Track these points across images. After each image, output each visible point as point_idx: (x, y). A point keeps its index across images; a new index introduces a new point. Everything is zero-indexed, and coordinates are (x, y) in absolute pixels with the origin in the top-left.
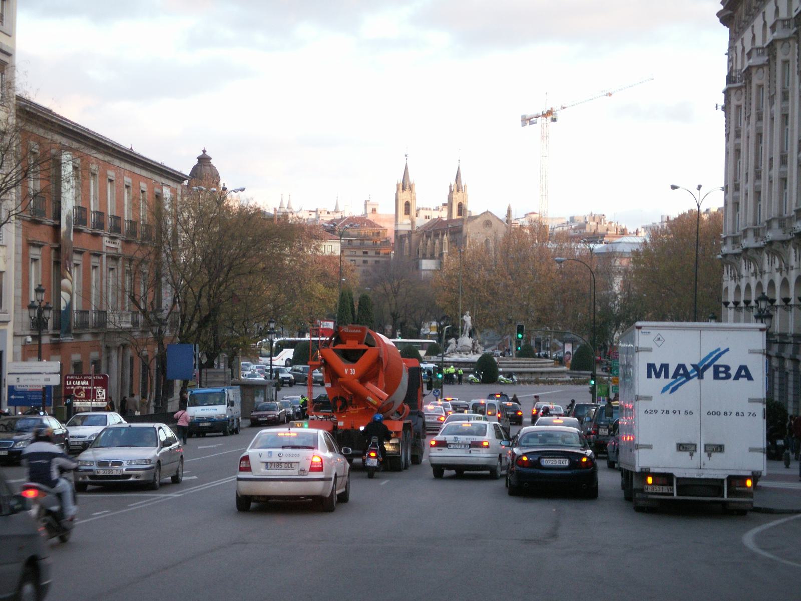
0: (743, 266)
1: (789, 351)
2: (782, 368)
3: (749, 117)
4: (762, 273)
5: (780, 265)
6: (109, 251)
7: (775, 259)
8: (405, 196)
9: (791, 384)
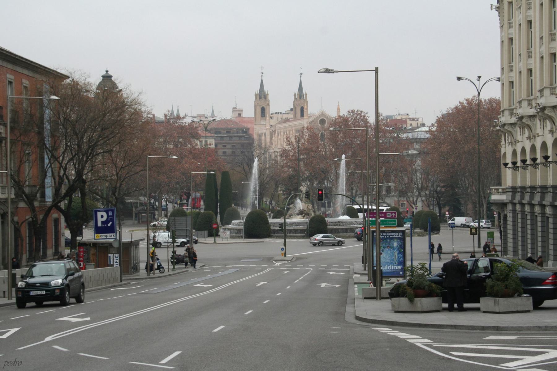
0: (519, 133)
1: (548, 199)
2: (523, 212)
3: (520, 8)
4: (516, 142)
5: (529, 135)
6: (446, 226)
7: (525, 130)
8: (262, 103)
9: (539, 224)
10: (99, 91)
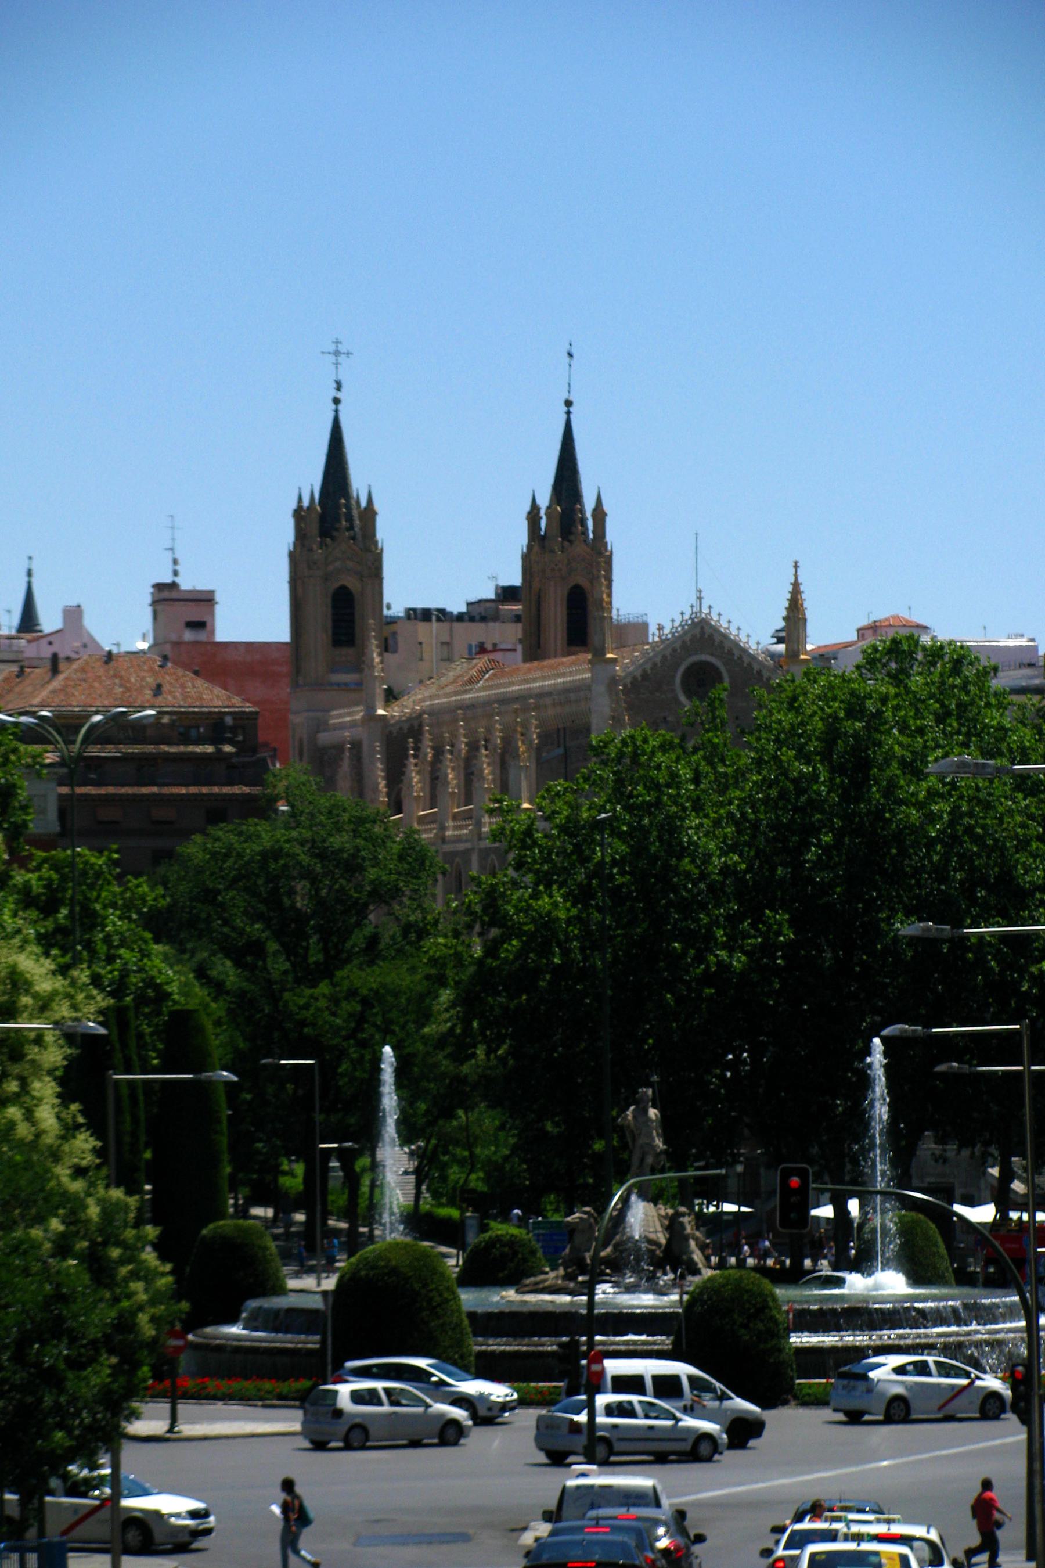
10: (560, 1030)
